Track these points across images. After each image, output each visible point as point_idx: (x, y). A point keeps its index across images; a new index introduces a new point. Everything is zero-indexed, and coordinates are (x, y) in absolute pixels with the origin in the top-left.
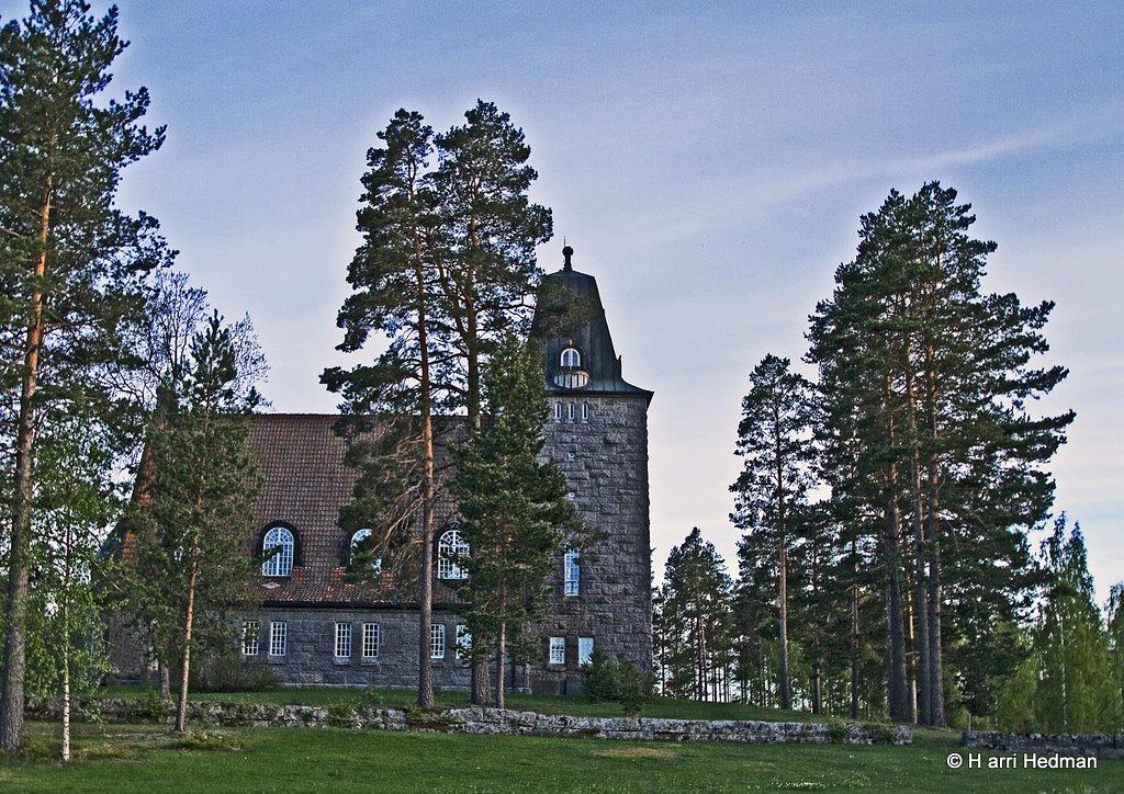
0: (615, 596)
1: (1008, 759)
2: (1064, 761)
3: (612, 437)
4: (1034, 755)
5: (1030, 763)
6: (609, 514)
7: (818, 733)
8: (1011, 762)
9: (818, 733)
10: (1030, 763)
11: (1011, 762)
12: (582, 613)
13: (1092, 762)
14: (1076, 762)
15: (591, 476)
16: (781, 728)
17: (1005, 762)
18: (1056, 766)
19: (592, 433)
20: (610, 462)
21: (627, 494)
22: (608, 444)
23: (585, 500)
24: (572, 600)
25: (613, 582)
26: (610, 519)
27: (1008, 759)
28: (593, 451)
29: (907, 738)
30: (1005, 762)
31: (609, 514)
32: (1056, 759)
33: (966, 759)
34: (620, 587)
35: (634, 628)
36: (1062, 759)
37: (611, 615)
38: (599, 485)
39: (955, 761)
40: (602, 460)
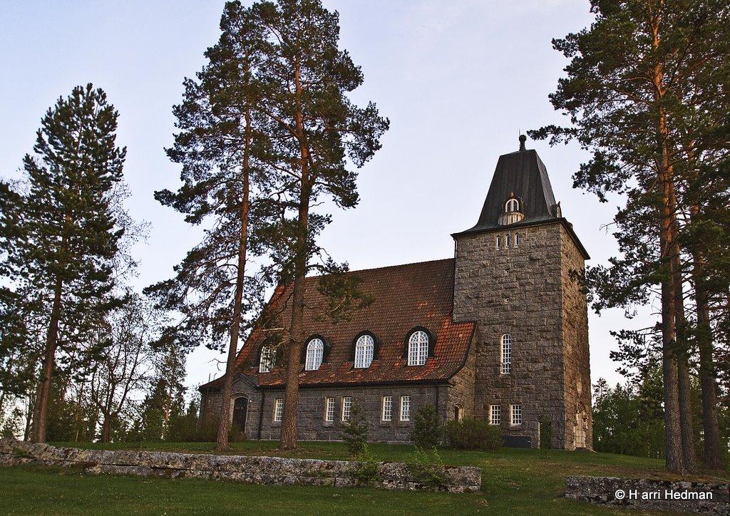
0: (537, 372)
1: (655, 493)
2: (691, 495)
3: (534, 255)
4: (672, 491)
5: (669, 496)
6: (533, 311)
7: (340, 474)
8: (657, 495)
9: (340, 474)
10: (669, 496)
11: (657, 495)
12: (513, 386)
13: (709, 495)
14: (699, 495)
15: (521, 285)
16: (295, 466)
17: (652, 495)
18: (686, 498)
19: (521, 254)
20: (534, 273)
21: (546, 295)
22: (532, 260)
23: (516, 303)
24: (505, 378)
25: (536, 362)
26: (533, 315)
27: (655, 493)
28: (521, 267)
29: (471, 484)
30: (652, 495)
31: (533, 311)
32: (686, 493)
33: (640, 497)
34: (540, 366)
35: (551, 396)
36: (689, 493)
37: (533, 387)
38: (525, 291)
39: (620, 494)
40: (529, 273)
